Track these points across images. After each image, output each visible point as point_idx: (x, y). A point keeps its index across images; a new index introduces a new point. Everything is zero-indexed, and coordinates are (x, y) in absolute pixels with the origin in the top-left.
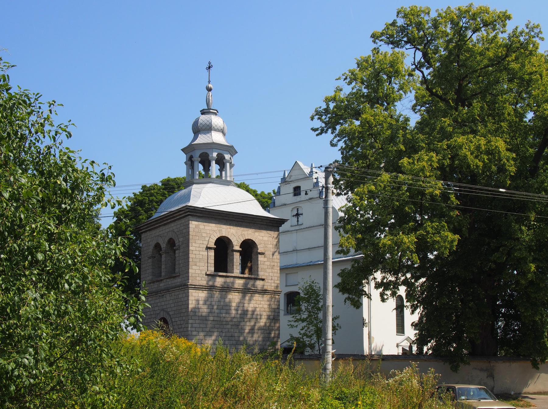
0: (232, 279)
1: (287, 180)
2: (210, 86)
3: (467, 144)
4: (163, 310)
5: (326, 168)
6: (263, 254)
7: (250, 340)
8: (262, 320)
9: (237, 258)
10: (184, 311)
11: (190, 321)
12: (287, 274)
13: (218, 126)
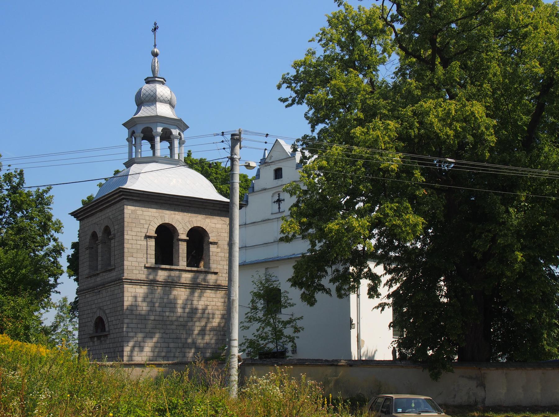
0: (178, 272)
1: (267, 161)
2: (156, 50)
3: (436, 110)
4: (100, 308)
5: (232, 135)
6: (215, 243)
7: (200, 342)
8: (214, 320)
9: (183, 248)
10: (119, 309)
11: (126, 321)
12: (267, 269)
13: (164, 97)
